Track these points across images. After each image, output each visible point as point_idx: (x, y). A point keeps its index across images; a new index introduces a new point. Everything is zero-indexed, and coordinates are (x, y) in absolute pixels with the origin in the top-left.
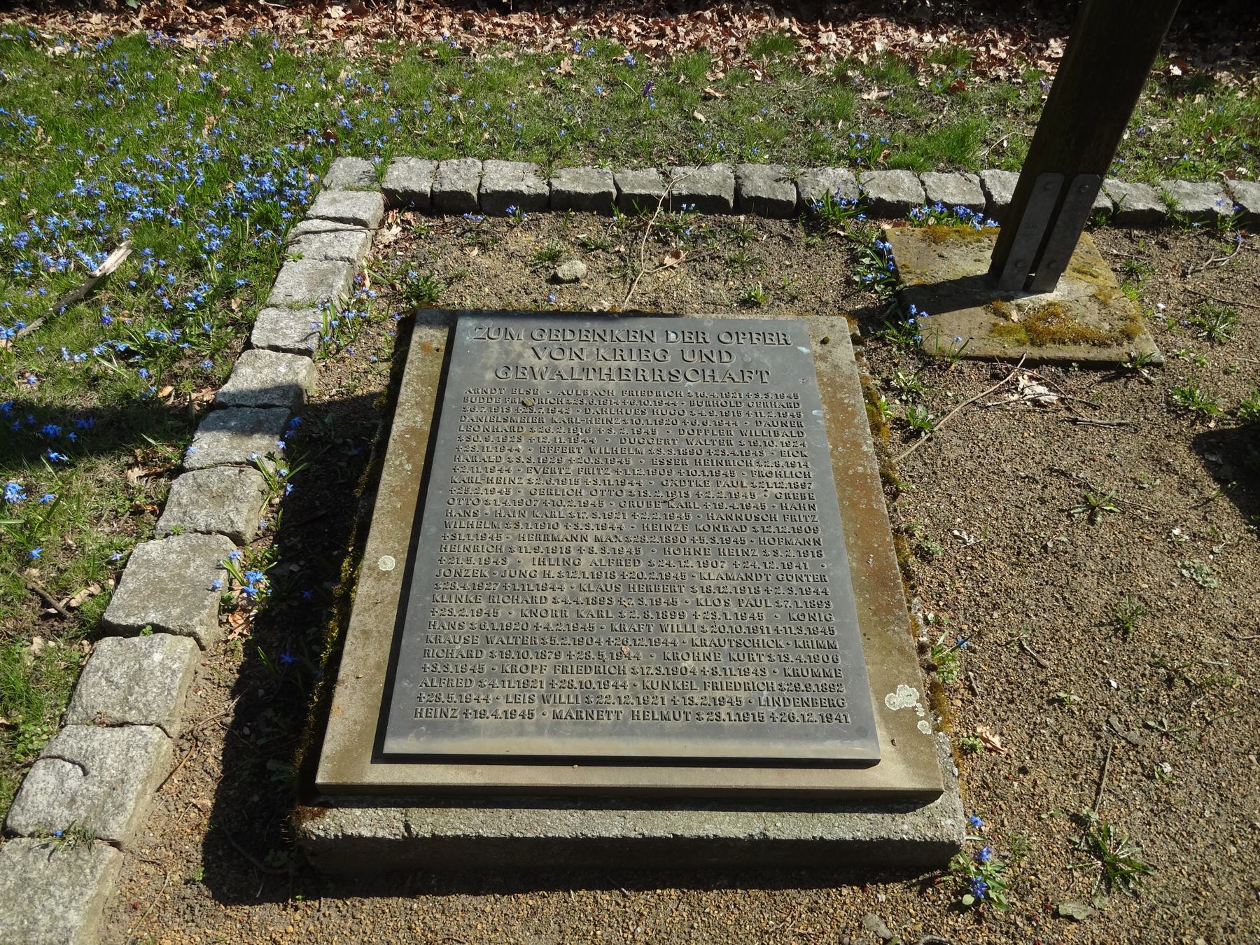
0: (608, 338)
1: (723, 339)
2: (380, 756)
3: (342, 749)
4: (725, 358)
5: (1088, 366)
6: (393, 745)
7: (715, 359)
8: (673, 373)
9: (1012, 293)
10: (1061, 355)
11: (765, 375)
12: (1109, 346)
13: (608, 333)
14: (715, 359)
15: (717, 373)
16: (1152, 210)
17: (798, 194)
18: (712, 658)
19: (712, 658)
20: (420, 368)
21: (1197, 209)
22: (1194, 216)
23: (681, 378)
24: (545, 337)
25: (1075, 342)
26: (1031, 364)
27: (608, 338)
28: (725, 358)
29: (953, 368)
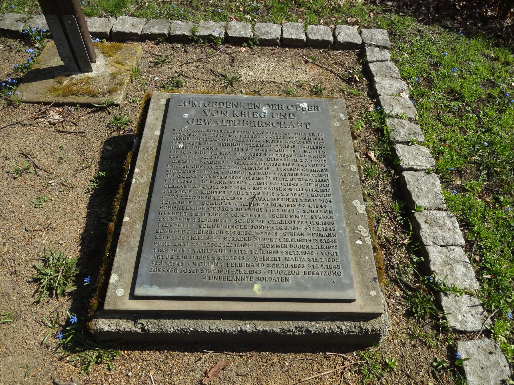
0: (239, 107)
1: (289, 108)
2: (133, 296)
3: (118, 292)
4: (292, 117)
5: (84, 106)
6: (139, 291)
7: (247, 115)
8: (268, 123)
9: (73, 73)
10: (72, 101)
11: (308, 125)
12: (97, 97)
13: (239, 104)
14: (287, 117)
15: (287, 124)
16: (184, 35)
17: (282, 35)
18: (270, 259)
19: (270, 259)
20: (154, 117)
21: (205, 34)
22: (203, 37)
23: (271, 126)
24: (211, 105)
25: (82, 95)
26: (58, 105)
27: (239, 107)
28: (292, 117)
29: (20, 107)
